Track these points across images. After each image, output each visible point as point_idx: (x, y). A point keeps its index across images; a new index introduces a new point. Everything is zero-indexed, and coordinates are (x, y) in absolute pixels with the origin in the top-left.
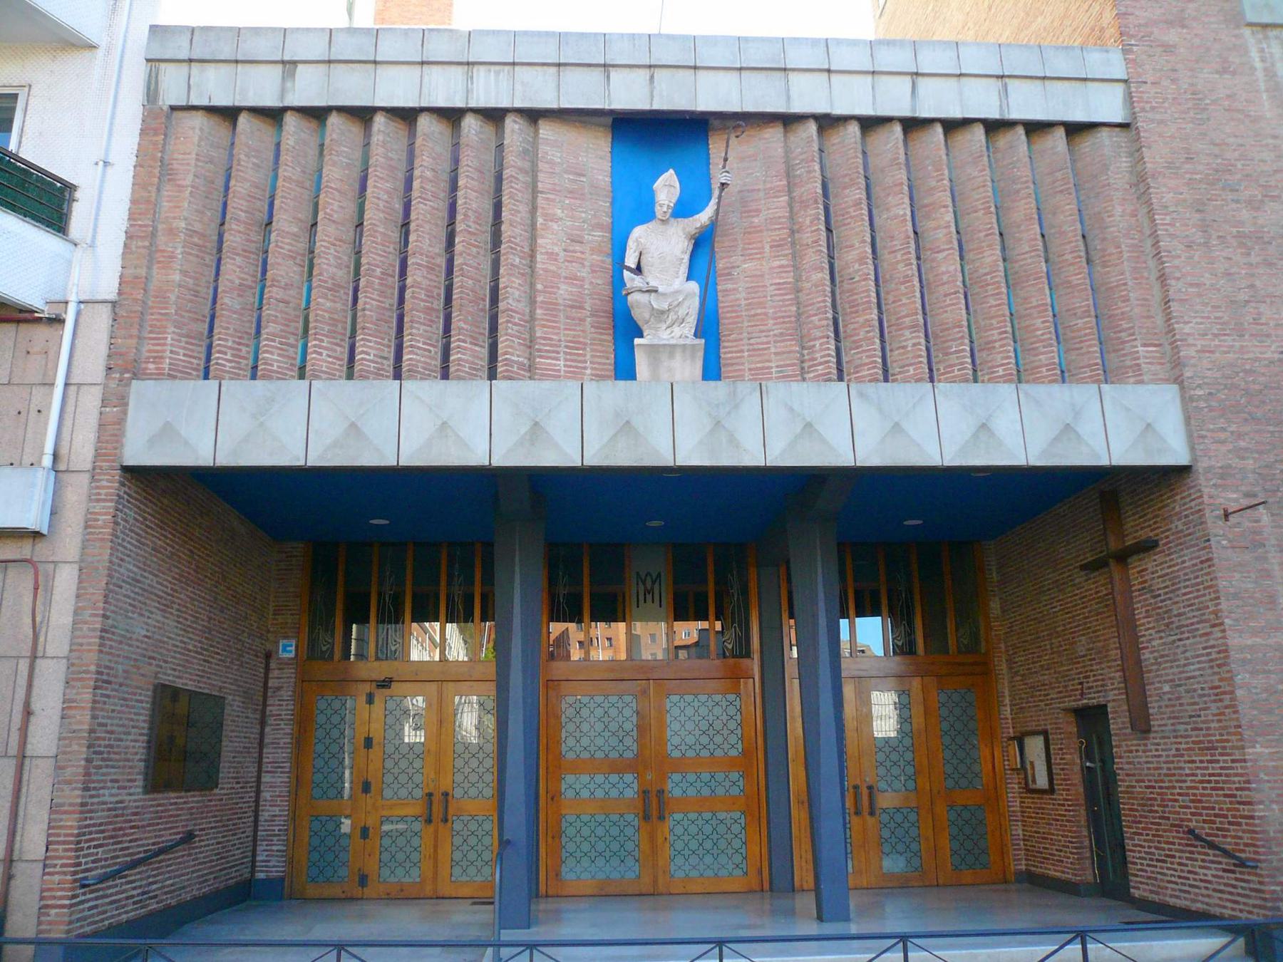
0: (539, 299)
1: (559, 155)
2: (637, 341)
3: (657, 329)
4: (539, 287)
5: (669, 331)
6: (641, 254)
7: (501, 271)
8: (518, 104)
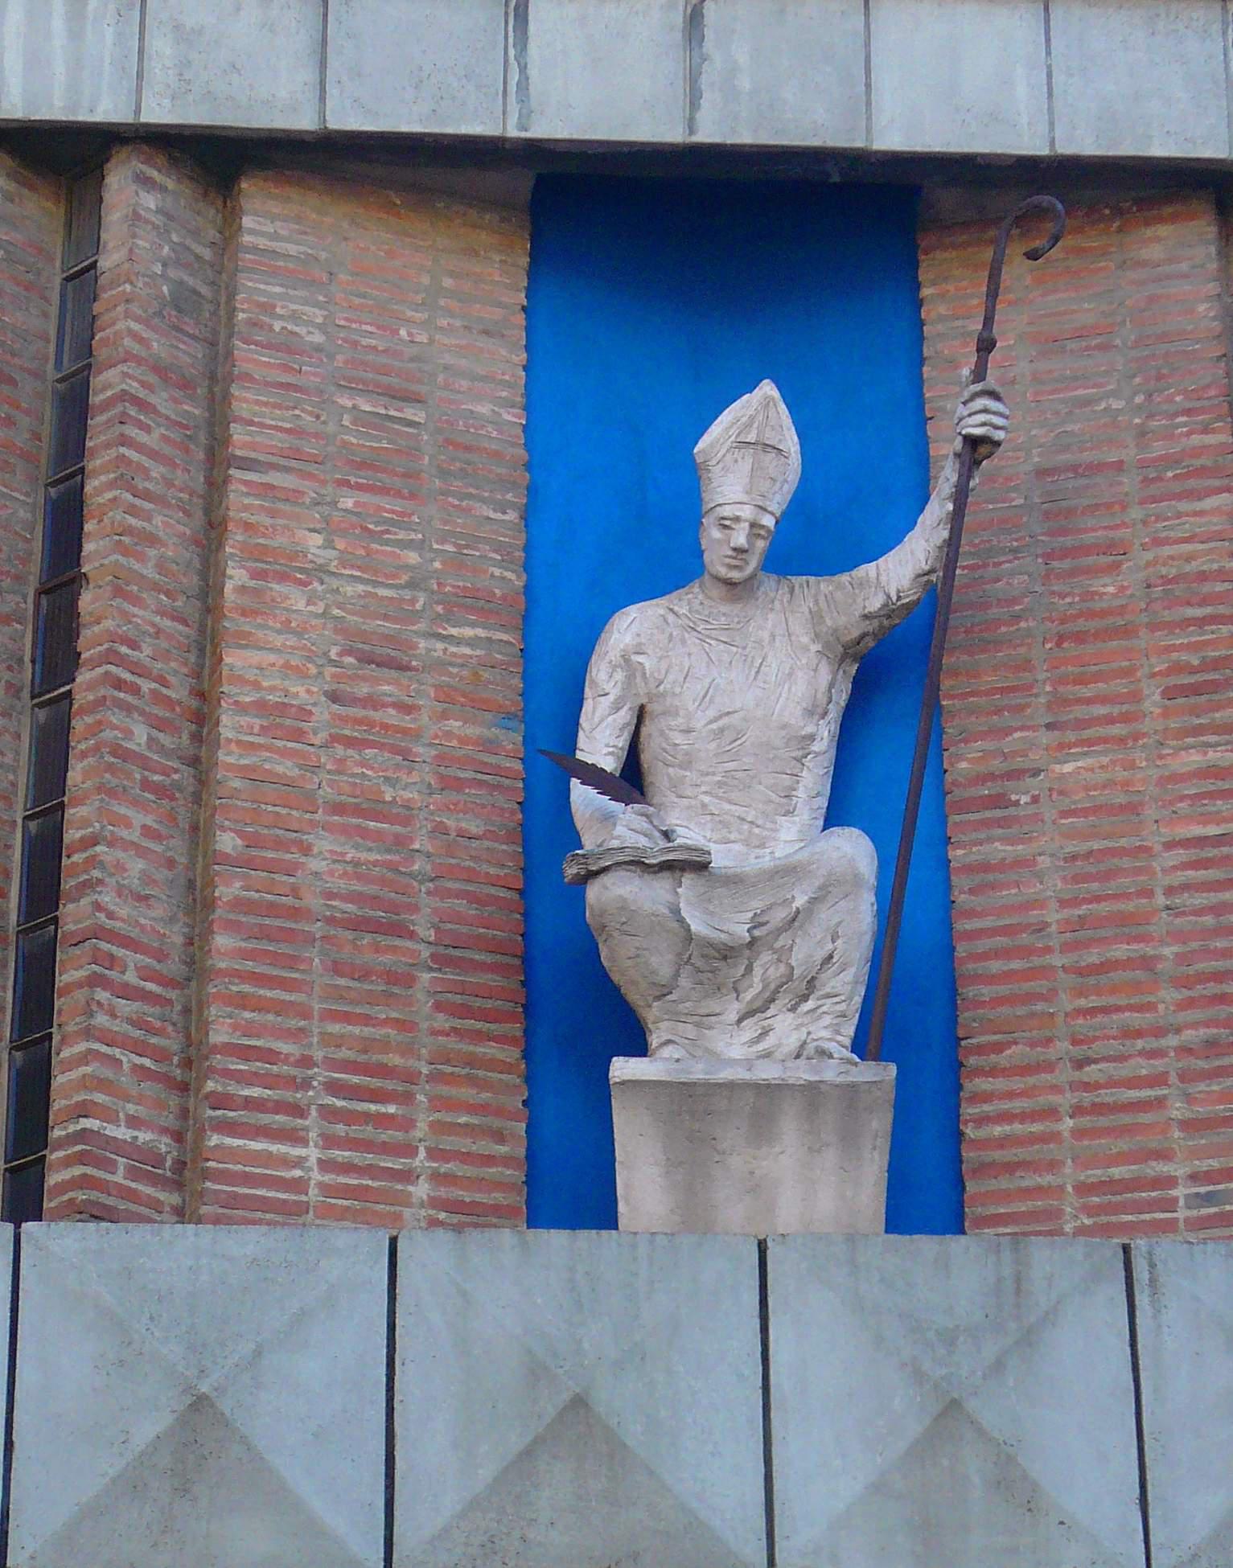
0: (227, 891)
1: (319, 316)
2: (622, 1068)
3: (703, 1021)
4: (227, 842)
5: (750, 1029)
6: (641, 714)
7: (74, 776)
8: (158, 112)
